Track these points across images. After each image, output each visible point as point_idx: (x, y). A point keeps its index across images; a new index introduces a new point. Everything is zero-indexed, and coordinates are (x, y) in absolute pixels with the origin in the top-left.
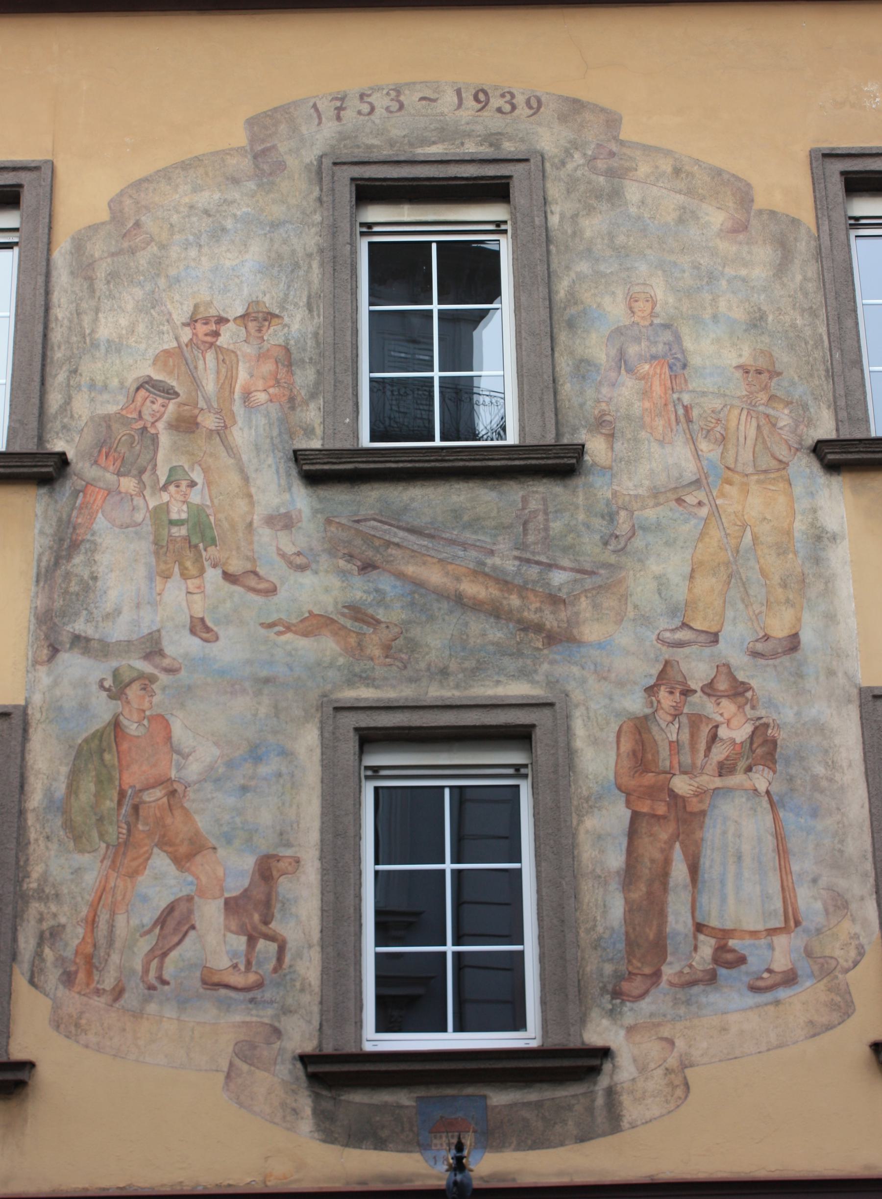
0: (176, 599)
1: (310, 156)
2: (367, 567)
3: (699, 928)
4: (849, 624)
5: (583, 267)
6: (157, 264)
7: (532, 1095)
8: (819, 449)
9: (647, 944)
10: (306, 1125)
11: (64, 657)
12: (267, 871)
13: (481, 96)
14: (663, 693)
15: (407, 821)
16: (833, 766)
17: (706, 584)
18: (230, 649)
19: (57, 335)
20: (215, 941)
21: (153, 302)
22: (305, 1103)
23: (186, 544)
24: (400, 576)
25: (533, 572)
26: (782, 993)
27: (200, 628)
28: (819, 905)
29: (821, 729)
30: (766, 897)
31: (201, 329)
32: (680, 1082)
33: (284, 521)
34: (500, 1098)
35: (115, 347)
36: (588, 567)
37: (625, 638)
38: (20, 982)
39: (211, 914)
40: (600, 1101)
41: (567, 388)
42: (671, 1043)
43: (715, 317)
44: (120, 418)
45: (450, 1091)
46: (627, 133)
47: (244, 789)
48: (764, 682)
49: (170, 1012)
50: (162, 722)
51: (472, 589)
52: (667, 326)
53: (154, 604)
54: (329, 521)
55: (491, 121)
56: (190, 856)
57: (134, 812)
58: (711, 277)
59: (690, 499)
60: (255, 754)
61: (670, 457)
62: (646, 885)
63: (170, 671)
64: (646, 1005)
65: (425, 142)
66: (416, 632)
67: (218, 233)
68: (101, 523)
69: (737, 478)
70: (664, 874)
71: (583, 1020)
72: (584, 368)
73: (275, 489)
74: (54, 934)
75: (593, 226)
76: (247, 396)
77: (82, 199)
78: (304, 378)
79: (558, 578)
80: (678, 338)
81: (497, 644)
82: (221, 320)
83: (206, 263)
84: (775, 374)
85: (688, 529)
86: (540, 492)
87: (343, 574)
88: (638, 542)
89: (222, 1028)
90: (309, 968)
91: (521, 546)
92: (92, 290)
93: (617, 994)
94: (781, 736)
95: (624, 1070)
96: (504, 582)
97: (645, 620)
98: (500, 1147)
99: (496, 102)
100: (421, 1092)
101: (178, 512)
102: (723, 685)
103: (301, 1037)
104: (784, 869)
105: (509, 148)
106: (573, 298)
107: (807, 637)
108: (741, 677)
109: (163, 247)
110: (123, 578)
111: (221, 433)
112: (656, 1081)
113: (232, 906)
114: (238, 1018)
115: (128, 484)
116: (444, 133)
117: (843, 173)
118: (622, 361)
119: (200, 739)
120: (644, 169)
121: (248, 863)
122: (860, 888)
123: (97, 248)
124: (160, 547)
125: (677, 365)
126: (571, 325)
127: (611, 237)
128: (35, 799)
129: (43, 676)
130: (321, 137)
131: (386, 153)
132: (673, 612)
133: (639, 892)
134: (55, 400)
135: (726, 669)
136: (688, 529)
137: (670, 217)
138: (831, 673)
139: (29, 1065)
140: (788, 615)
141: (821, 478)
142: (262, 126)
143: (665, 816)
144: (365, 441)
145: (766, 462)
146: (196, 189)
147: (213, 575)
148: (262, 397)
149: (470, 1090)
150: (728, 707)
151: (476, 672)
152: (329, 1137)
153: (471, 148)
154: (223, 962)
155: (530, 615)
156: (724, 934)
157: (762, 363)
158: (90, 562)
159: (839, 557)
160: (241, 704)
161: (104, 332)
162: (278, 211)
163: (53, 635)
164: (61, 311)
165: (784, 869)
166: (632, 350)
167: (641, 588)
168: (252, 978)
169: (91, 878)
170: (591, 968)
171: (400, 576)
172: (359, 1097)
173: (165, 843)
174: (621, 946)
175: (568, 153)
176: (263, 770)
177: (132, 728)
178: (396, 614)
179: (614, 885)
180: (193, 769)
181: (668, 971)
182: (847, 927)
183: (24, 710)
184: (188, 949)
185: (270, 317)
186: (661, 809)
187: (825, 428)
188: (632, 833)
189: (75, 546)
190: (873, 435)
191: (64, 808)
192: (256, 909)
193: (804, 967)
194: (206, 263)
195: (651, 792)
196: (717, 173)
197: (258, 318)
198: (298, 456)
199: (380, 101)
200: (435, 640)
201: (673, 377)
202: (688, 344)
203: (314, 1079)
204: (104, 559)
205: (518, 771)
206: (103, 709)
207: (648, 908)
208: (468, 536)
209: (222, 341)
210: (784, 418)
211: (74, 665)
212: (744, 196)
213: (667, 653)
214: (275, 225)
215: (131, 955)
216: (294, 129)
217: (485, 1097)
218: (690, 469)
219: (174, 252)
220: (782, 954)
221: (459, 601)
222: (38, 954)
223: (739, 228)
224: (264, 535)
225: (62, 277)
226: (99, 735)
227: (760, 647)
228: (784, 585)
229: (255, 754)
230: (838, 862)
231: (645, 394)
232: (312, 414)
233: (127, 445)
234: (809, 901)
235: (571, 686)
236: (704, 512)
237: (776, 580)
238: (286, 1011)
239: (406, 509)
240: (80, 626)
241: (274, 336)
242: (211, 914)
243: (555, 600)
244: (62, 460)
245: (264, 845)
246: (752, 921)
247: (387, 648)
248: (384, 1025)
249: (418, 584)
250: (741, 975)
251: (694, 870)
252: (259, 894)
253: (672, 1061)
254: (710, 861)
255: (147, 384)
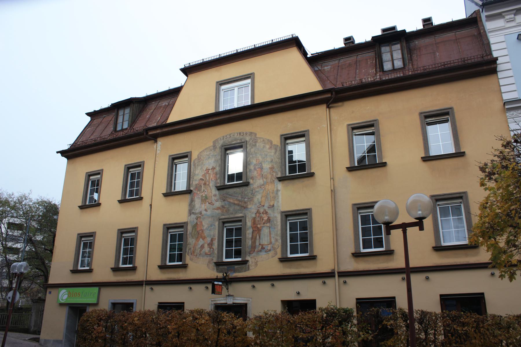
0: (203, 207)
1: (220, 145)
2: (224, 200)
3: (260, 244)
5: (251, 156)
6: (202, 163)
7: (239, 266)
8: (278, 178)
9: (253, 247)
10: (215, 270)
12: (212, 240)
13: (240, 134)
15: (230, 232)
16: (277, 222)
17: (263, 198)
18: (209, 213)
19: (191, 174)
20: (206, 249)
21: (202, 168)
22: (215, 268)
23: (204, 200)
25: (243, 199)
27: (206, 210)
29: (276, 217)
32: (256, 264)
33: (215, 195)
34: (236, 267)
35: (198, 175)
37: (253, 207)
38: (187, 255)
39: (206, 245)
41: (248, 173)
44: (198, 184)
46: (257, 136)
48: (269, 211)
50: (201, 222)
51: (236, 202)
55: (241, 137)
57: (199, 234)
58: (267, 155)
60: (211, 226)
61: (260, 182)
62: (254, 239)
64: (253, 255)
68: (196, 198)
70: (256, 238)
71: (246, 257)
72: (250, 170)
73: (214, 191)
74: (190, 249)
75: (252, 150)
77: (194, 156)
78: (218, 176)
79: (246, 200)
84: (274, 168)
89: (207, 259)
90: (216, 252)
93: (250, 253)
94: (271, 218)
96: (239, 201)
97: (256, 204)
103: (215, 260)
104: (270, 236)
105: (243, 140)
106: (250, 161)
110: (198, 205)
111: (209, 185)
113: (208, 245)
115: (199, 192)
116: (236, 140)
118: (255, 169)
119: (205, 224)
120: (259, 141)
121: (210, 239)
123: (196, 162)
124: (202, 200)
125: (261, 168)
126: (249, 164)
128: (188, 233)
129: (189, 218)
130: (221, 142)
131: (229, 144)
132: (259, 203)
133: (253, 240)
134: (191, 182)
135: (265, 210)
136: (261, 191)
140: (273, 202)
141: (278, 182)
142: (214, 142)
143: (257, 230)
144: (287, 174)
145: (272, 181)
147: (207, 203)
150: (265, 215)
151: (236, 213)
152: (218, 272)
153: (238, 141)
154: (207, 251)
156: (263, 245)
159: (280, 193)
160: (210, 219)
161: (197, 173)
162: (216, 154)
163: (191, 213)
164: (192, 171)
165: (270, 236)
166: (256, 167)
167: (255, 200)
169: (194, 242)
172: (221, 267)
173: (202, 237)
178: (227, 206)
180: (205, 228)
182: (277, 243)
183: (187, 222)
184: (204, 250)
185: (215, 168)
187: (279, 175)
188: (253, 233)
190: (431, 155)
191: (191, 234)
192: (211, 245)
195: (255, 227)
196: (268, 140)
197: (213, 168)
198: (216, 187)
199: (228, 136)
200: (231, 209)
204: (196, 202)
205: (461, 203)
206: (195, 221)
207: (254, 242)
211: (193, 216)
212: (271, 142)
218: (262, 183)
220: (269, 247)
221: (234, 204)
223: (271, 148)
224: (213, 197)
225: (192, 166)
230: (277, 235)
231: (257, 173)
232: (219, 181)
233: (198, 187)
234: (273, 240)
240: (193, 211)
241: (215, 171)
243: (245, 203)
244: (191, 191)
246: (266, 243)
248: (364, 248)
249: (230, 202)
250: (264, 250)
251: (260, 237)
255: (201, 179)
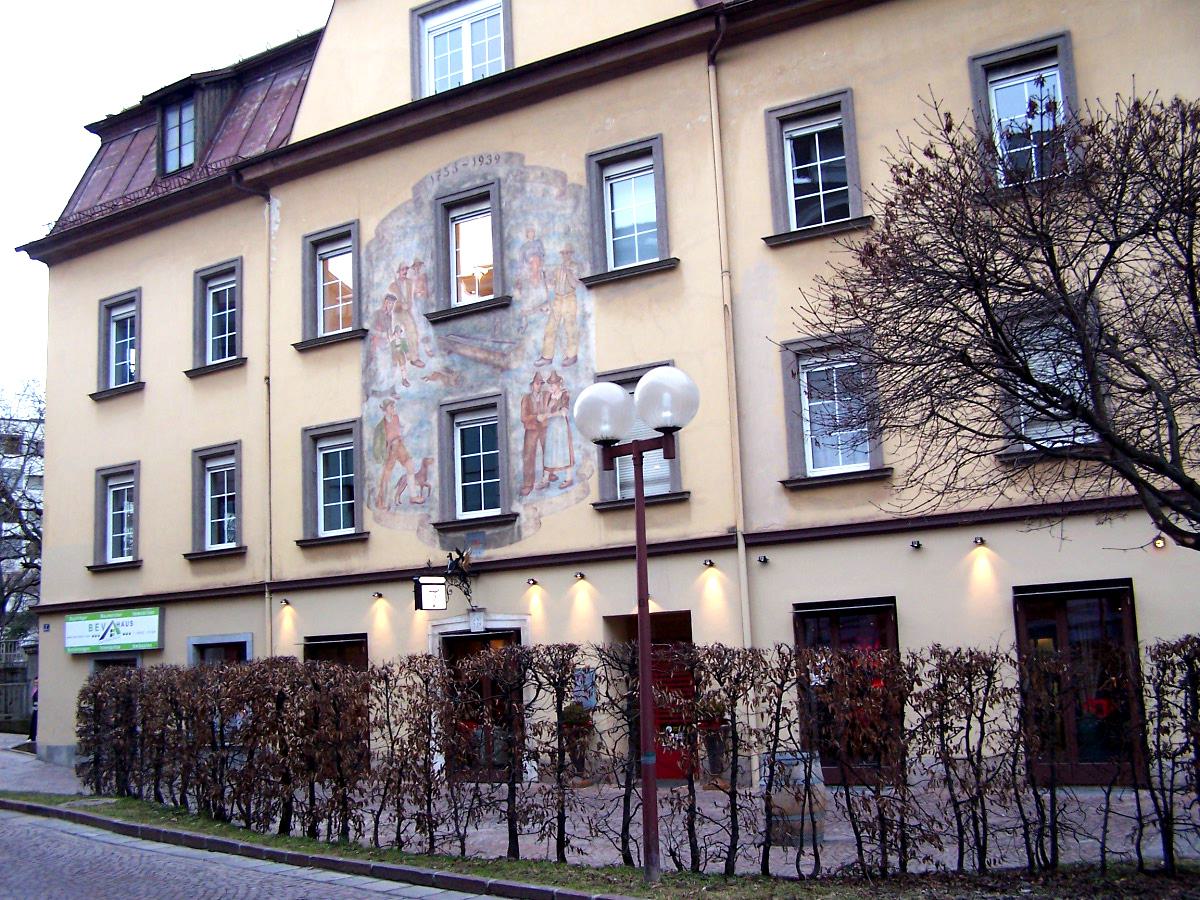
2: (450, 352)
3: (545, 468)
4: (593, 349)
6: (389, 250)
7: (497, 530)
10: (438, 545)
11: (370, 399)
12: (425, 464)
13: (481, 159)
14: (535, 385)
18: (413, 389)
19: (364, 284)
20: (413, 489)
23: (400, 354)
24: (459, 354)
25: (497, 345)
26: (568, 489)
27: (405, 383)
28: (580, 456)
30: (564, 455)
31: (402, 273)
33: (426, 340)
34: (488, 532)
36: (513, 340)
38: (365, 507)
39: (411, 480)
40: (516, 530)
41: (508, 272)
42: (536, 509)
43: (554, 233)
45: (475, 531)
47: (419, 437)
48: (566, 376)
49: (402, 513)
50: (396, 416)
51: (480, 355)
52: (538, 240)
53: (393, 376)
54: (439, 338)
55: (485, 168)
56: (406, 461)
58: (553, 216)
59: (545, 309)
62: (529, 454)
63: (398, 399)
64: (529, 497)
65: (464, 182)
66: (463, 374)
67: (405, 235)
68: (378, 349)
69: (559, 297)
70: (535, 451)
72: (513, 262)
73: (425, 329)
76: (415, 294)
78: (431, 284)
79: (504, 346)
80: (542, 244)
81: (487, 374)
82: (407, 268)
83: (402, 247)
84: (572, 252)
85: (544, 320)
86: (499, 315)
87: (443, 356)
88: (528, 329)
89: (416, 515)
91: (493, 336)
92: (372, 264)
95: (522, 520)
96: (489, 351)
98: (489, 548)
99: (486, 160)
100: (467, 532)
101: (398, 342)
102: (553, 379)
105: (490, 178)
107: (580, 356)
108: (559, 375)
109: (390, 244)
110: (388, 372)
111: (408, 311)
112: (532, 523)
114: (419, 513)
115: (384, 334)
116: (471, 177)
117: (597, 162)
118: (525, 258)
119: (407, 419)
120: (532, 176)
121: (420, 461)
122: (301, 894)
123: (373, 249)
126: (509, 247)
127: (521, 207)
130: (433, 189)
131: (455, 191)
134: (364, 308)
136: (544, 320)
137: (540, 195)
138: (587, 368)
139: (369, 533)
140: (574, 348)
141: (586, 292)
142: (416, 189)
143: (536, 429)
145: (569, 289)
146: (399, 219)
147: (408, 363)
148: (419, 295)
149: (480, 530)
150: (555, 386)
151: (480, 386)
155: (496, 362)
157: (569, 250)
158: (376, 365)
159: (591, 323)
161: (376, 280)
163: (368, 392)
164: (364, 275)
167: (529, 346)
168: (422, 499)
169: (381, 472)
170: (514, 486)
171: (459, 354)
173: (399, 458)
174: (522, 477)
175: (508, 175)
176: (424, 429)
177: (389, 420)
179: (520, 456)
180: (405, 431)
181: (536, 485)
182: (589, 463)
183: (361, 419)
185: (421, 263)
186: (534, 427)
188: (526, 438)
189: (371, 359)
191: (371, 449)
192: (422, 476)
193: (576, 478)
194: (402, 247)
195: (531, 422)
197: (418, 264)
200: (469, 376)
201: (540, 260)
202: (545, 246)
203: (191, 561)
204: (379, 363)
206: (381, 414)
207: (530, 463)
208: (479, 335)
209: (408, 276)
210: (575, 270)
211: (375, 402)
213: (537, 369)
214: (421, 228)
215: (391, 496)
216: (426, 188)
217: (484, 532)
219: (394, 245)
220: (569, 475)
222: (369, 497)
223: (562, 194)
224: (421, 345)
226: (380, 424)
227: (566, 362)
228: (573, 337)
229: (421, 424)
231: (531, 269)
235: (508, 386)
236: (549, 312)
237: (571, 335)
238: (432, 509)
239: (461, 329)
240: (374, 387)
241: (422, 271)
242: (411, 480)
243: (504, 355)
245: (424, 455)
246: (560, 465)
247: (456, 381)
250: (557, 483)
252: (423, 472)
253: (537, 515)
254: (549, 443)
